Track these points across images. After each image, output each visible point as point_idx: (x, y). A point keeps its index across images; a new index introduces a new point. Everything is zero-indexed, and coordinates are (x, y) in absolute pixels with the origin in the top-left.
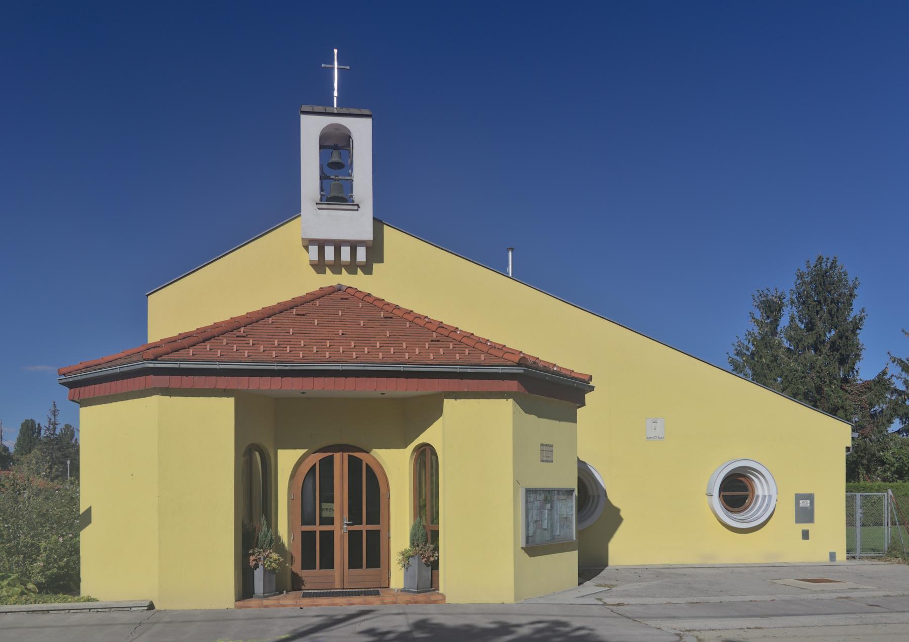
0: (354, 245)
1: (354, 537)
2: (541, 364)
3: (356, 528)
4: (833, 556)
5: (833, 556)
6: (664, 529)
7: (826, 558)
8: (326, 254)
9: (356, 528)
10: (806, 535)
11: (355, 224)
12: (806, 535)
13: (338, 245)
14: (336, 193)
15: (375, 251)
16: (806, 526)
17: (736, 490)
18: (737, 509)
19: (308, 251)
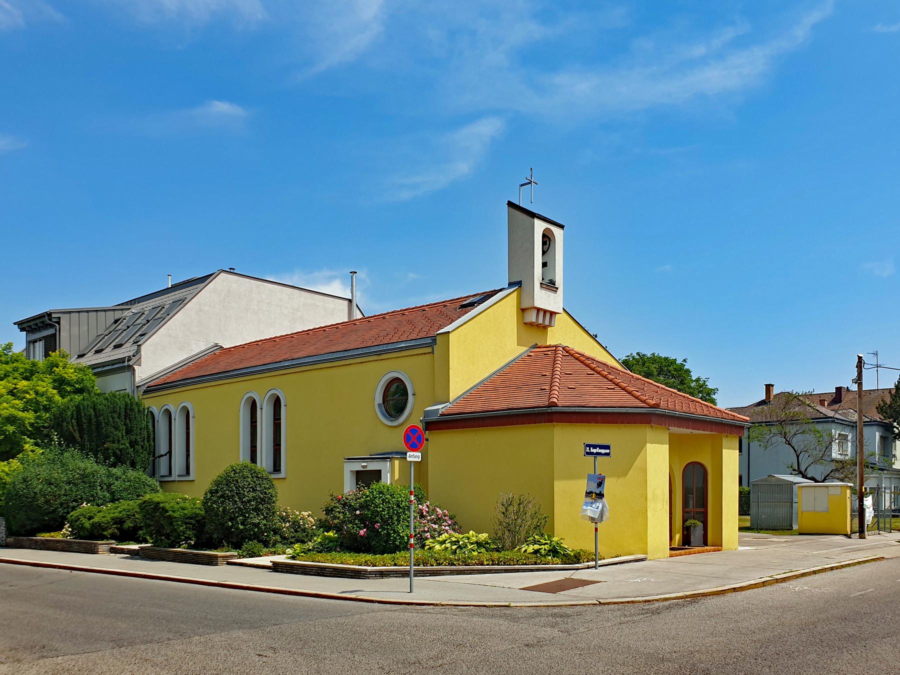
13: (545, 311)
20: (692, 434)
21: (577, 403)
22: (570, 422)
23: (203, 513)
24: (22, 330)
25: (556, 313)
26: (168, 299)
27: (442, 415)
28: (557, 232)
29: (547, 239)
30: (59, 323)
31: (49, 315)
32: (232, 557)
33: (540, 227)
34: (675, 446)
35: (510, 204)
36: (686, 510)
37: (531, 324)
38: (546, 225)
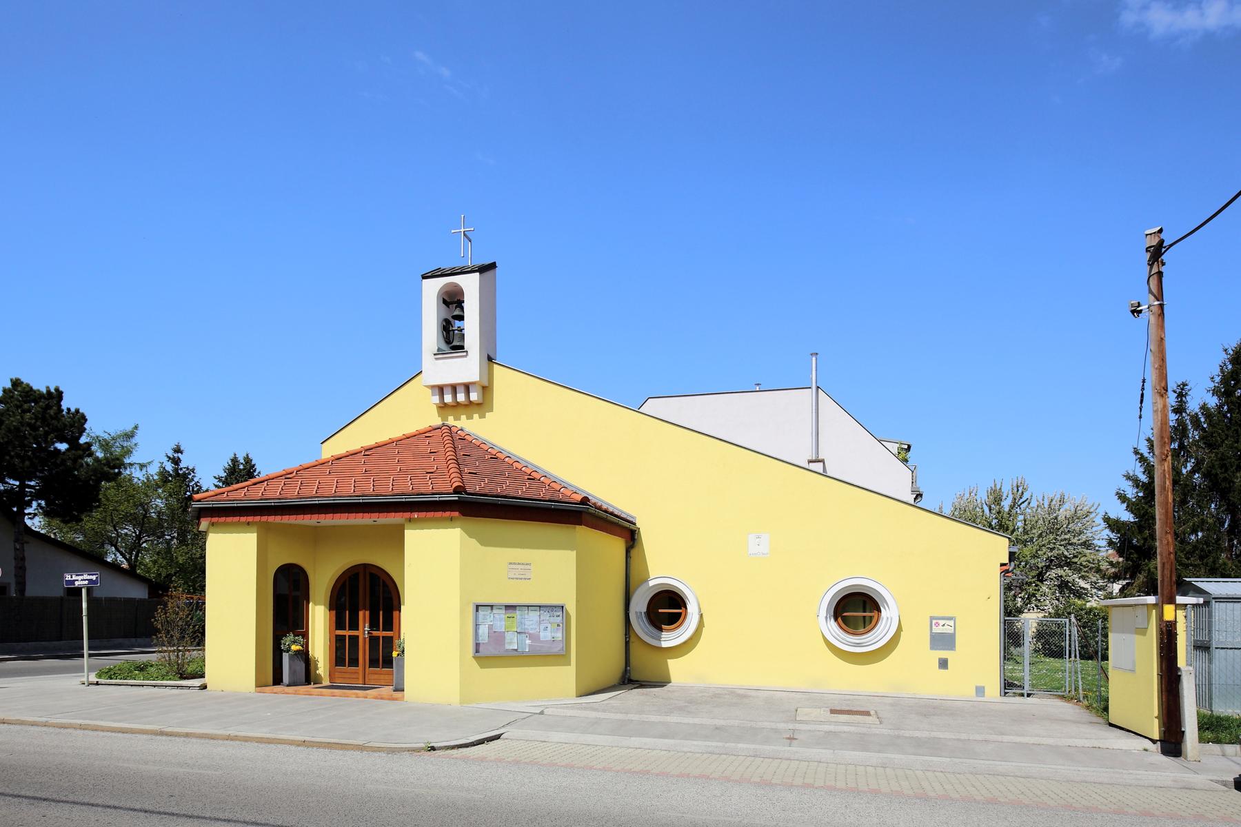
0: (467, 387)
1: (374, 641)
2: (395, 613)
3: (375, 633)
4: (980, 691)
5: (980, 691)
6: (752, 637)
7: (970, 692)
8: (457, 399)
9: (375, 633)
10: (943, 664)
11: (465, 368)
12: (943, 664)
13: (454, 388)
14: (452, 340)
15: (486, 389)
16: (943, 654)
17: (856, 608)
18: (850, 630)
19: (966, 516)
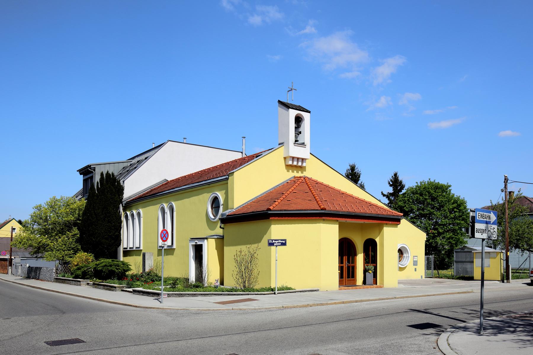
13: (298, 159)
20: (364, 224)
21: (284, 208)
22: (361, 219)
23: (206, 285)
24: (81, 174)
25: (306, 159)
26: (143, 157)
27: (227, 216)
28: (305, 115)
29: (298, 120)
30: (94, 170)
31: (89, 166)
32: (123, 287)
33: (293, 113)
34: (341, 228)
35: (279, 101)
36: (375, 264)
37: (291, 166)
38: (296, 112)
